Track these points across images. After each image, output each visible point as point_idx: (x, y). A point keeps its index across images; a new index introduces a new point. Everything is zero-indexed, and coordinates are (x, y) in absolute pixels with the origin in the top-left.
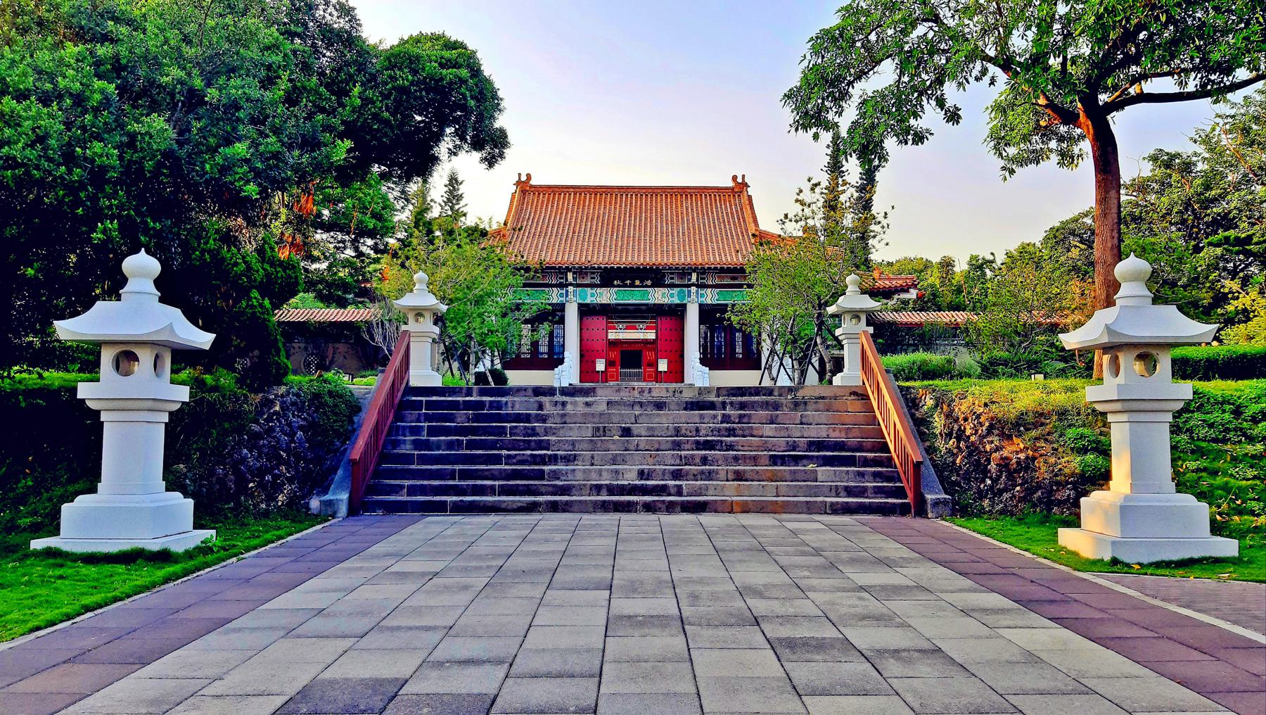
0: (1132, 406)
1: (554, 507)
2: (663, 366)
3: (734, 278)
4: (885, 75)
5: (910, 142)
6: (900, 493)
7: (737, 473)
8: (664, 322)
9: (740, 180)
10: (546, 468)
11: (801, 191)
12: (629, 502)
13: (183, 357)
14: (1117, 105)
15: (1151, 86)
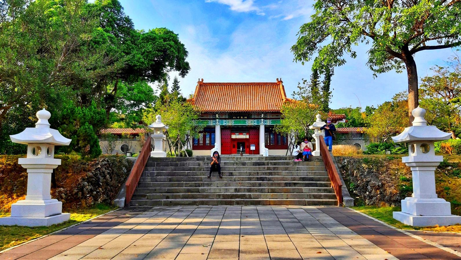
0: (421, 165)
1: (202, 203)
2: (253, 148)
3: (277, 116)
4: (329, 41)
5: (337, 66)
6: (334, 197)
7: (272, 189)
8: (253, 132)
9: (279, 80)
10: (200, 188)
11: (299, 84)
12: (231, 201)
13: (59, 149)
14: (414, 50)
15: (428, 43)
